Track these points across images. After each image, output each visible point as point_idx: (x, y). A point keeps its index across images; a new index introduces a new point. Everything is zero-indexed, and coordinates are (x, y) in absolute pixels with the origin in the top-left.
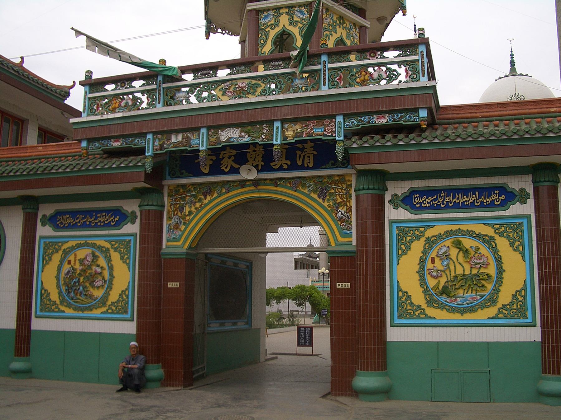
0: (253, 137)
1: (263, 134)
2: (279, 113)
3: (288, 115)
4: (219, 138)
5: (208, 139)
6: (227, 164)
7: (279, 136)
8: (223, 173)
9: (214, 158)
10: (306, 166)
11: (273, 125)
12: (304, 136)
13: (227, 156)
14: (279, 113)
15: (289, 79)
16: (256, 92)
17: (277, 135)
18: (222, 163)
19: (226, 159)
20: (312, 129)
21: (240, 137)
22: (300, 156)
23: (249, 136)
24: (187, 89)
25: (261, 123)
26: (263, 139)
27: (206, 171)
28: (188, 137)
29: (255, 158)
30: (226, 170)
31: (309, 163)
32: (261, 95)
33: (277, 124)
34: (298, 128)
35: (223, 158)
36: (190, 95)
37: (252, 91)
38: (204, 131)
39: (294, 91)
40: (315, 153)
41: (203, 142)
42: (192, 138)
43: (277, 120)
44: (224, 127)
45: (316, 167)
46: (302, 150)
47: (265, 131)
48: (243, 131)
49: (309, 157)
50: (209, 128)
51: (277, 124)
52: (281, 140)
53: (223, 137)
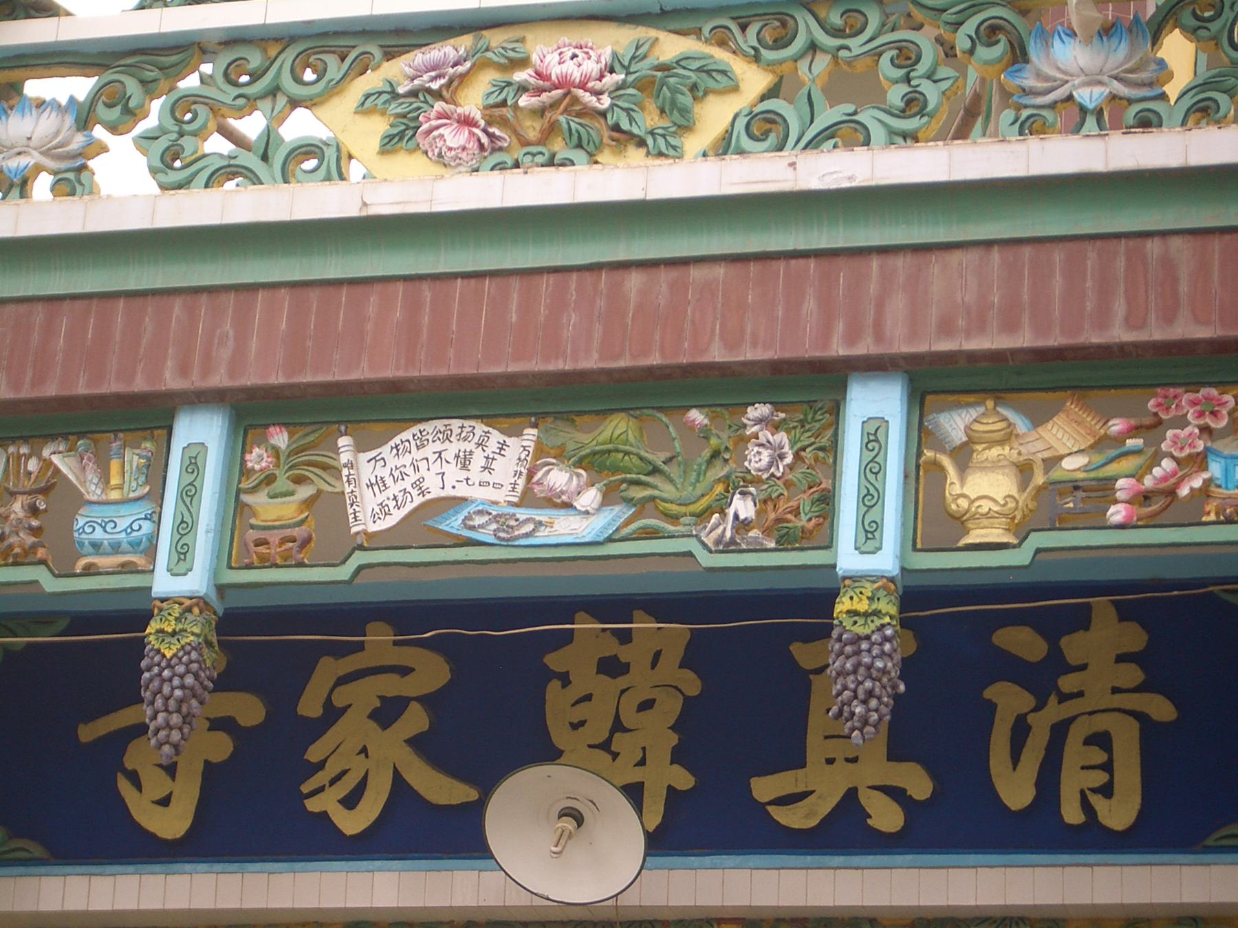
0: (642, 507)
1: (740, 482)
2: (898, 305)
3: (979, 325)
4: (330, 508)
5: (236, 509)
6: (361, 762)
7: (886, 507)
8: (319, 843)
9: (249, 710)
10: (1072, 814)
11: (836, 410)
12: (1117, 513)
13: (365, 695)
14: (898, 305)
15: (990, 33)
16: (686, 126)
17: (870, 499)
18: (314, 753)
19: (355, 728)
20: (1199, 461)
21: (528, 499)
22: (1020, 731)
23: (608, 498)
24: (80, 87)
25: (726, 386)
26: (742, 525)
27: (171, 824)
28: (51, 484)
29: (618, 726)
30: (352, 823)
31: (1106, 791)
32: (724, 146)
33: (875, 404)
34: (1064, 441)
35: (332, 714)
36: (99, 132)
37: (649, 119)
38: (202, 432)
39: (1030, 127)
40: (1161, 709)
41: (185, 527)
42: (93, 491)
43: (876, 366)
44: (386, 406)
45: (1154, 835)
46: (1042, 679)
47: (757, 459)
48: (561, 455)
49: (1102, 740)
50: (250, 411)
51: (875, 404)
52: (914, 542)
53: (370, 501)
